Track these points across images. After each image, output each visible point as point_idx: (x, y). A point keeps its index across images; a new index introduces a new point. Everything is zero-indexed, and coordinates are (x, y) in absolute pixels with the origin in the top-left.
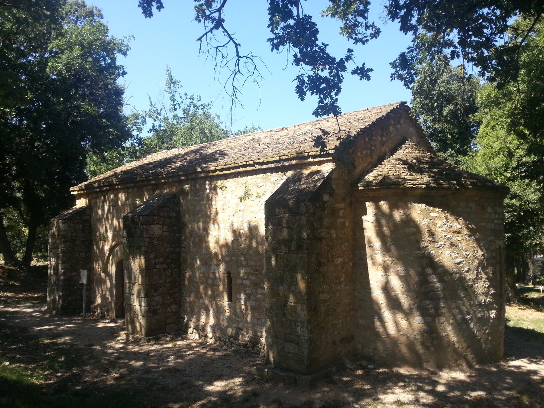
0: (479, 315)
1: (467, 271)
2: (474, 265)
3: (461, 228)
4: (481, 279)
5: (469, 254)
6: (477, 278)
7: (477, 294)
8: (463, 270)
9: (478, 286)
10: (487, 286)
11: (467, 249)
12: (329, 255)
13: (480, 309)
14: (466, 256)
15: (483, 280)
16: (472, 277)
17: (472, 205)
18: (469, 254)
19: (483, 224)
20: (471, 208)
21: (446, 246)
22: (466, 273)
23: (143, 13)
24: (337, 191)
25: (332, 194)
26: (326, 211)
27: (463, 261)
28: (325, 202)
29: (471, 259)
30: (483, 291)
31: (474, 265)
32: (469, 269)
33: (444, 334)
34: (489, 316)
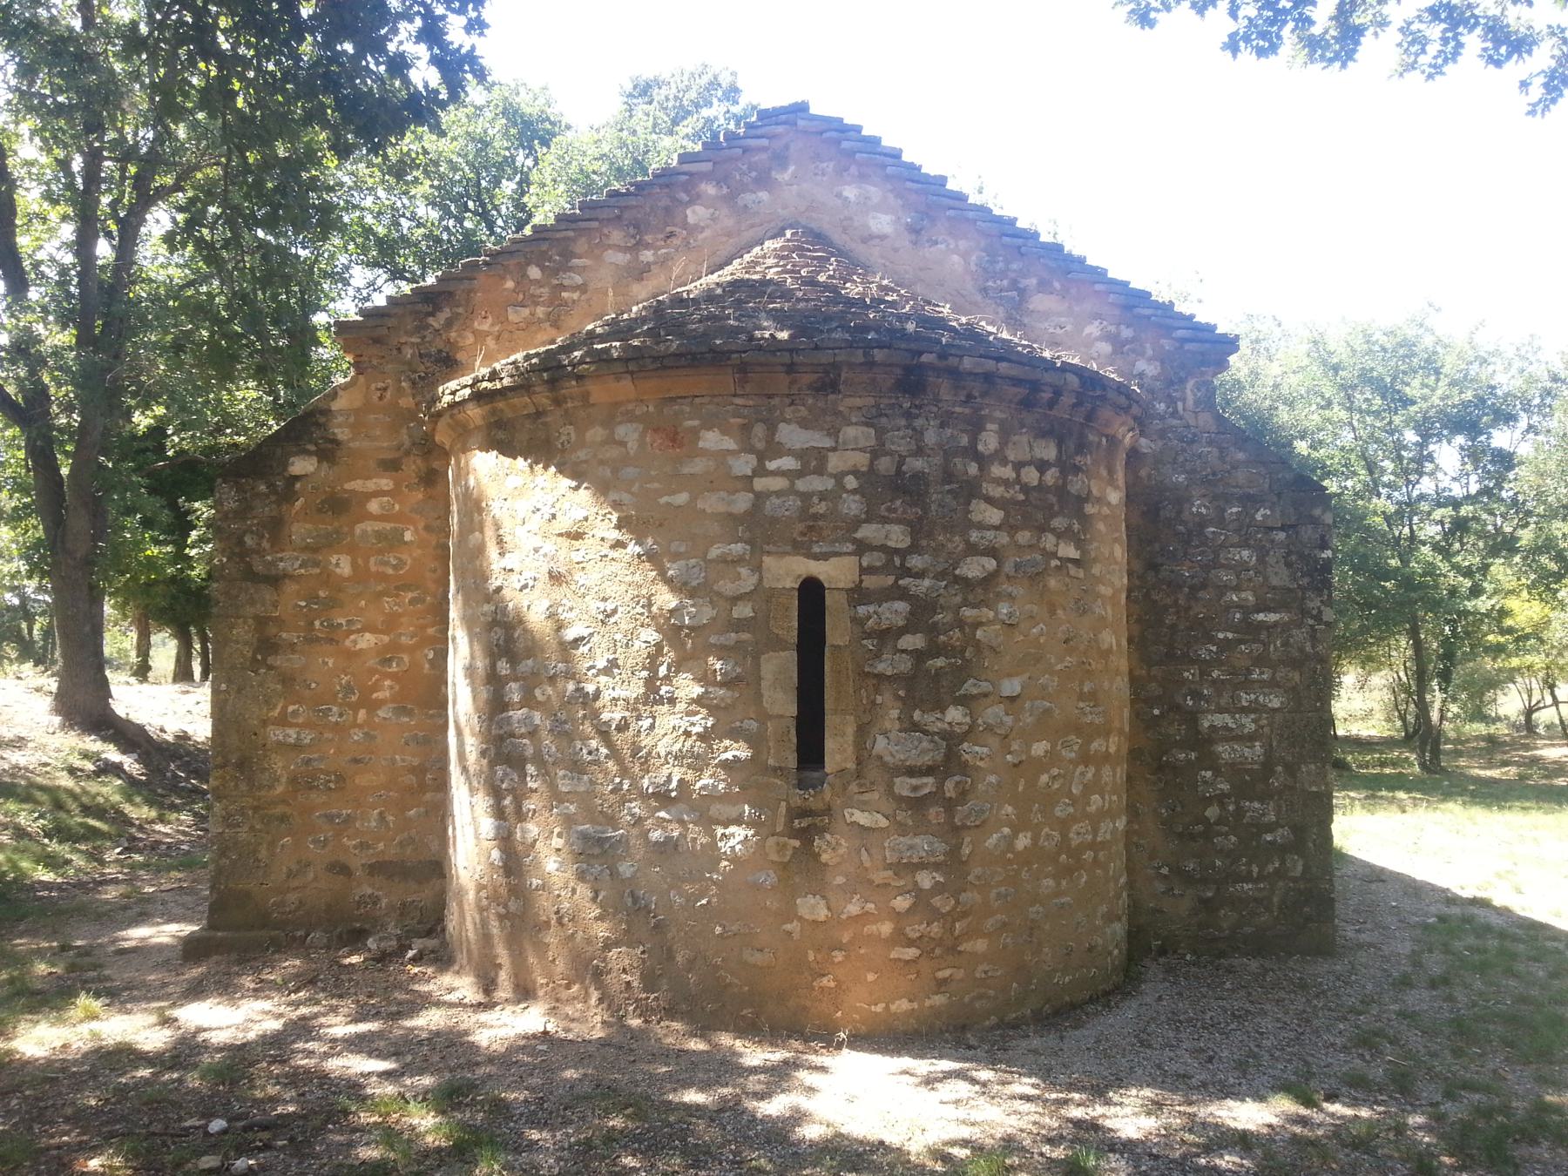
0: (656, 835)
1: (607, 671)
2: (636, 647)
3: (586, 519)
4: (672, 701)
5: (615, 611)
6: (652, 695)
7: (649, 753)
8: (592, 667)
9: (652, 727)
10: (698, 729)
11: (609, 593)
12: (317, 623)
13: (662, 814)
14: (601, 617)
15: (681, 707)
16: (623, 694)
17: (628, 433)
18: (615, 611)
19: (682, 498)
20: (623, 444)
21: (539, 585)
22: (603, 679)
23: (801, 108)
24: (355, 445)
25: (329, 452)
26: (298, 504)
27: (591, 635)
28: (297, 478)
29: (624, 626)
30: (677, 746)
31: (636, 647)
32: (613, 664)
33: (536, 882)
34: (713, 845)
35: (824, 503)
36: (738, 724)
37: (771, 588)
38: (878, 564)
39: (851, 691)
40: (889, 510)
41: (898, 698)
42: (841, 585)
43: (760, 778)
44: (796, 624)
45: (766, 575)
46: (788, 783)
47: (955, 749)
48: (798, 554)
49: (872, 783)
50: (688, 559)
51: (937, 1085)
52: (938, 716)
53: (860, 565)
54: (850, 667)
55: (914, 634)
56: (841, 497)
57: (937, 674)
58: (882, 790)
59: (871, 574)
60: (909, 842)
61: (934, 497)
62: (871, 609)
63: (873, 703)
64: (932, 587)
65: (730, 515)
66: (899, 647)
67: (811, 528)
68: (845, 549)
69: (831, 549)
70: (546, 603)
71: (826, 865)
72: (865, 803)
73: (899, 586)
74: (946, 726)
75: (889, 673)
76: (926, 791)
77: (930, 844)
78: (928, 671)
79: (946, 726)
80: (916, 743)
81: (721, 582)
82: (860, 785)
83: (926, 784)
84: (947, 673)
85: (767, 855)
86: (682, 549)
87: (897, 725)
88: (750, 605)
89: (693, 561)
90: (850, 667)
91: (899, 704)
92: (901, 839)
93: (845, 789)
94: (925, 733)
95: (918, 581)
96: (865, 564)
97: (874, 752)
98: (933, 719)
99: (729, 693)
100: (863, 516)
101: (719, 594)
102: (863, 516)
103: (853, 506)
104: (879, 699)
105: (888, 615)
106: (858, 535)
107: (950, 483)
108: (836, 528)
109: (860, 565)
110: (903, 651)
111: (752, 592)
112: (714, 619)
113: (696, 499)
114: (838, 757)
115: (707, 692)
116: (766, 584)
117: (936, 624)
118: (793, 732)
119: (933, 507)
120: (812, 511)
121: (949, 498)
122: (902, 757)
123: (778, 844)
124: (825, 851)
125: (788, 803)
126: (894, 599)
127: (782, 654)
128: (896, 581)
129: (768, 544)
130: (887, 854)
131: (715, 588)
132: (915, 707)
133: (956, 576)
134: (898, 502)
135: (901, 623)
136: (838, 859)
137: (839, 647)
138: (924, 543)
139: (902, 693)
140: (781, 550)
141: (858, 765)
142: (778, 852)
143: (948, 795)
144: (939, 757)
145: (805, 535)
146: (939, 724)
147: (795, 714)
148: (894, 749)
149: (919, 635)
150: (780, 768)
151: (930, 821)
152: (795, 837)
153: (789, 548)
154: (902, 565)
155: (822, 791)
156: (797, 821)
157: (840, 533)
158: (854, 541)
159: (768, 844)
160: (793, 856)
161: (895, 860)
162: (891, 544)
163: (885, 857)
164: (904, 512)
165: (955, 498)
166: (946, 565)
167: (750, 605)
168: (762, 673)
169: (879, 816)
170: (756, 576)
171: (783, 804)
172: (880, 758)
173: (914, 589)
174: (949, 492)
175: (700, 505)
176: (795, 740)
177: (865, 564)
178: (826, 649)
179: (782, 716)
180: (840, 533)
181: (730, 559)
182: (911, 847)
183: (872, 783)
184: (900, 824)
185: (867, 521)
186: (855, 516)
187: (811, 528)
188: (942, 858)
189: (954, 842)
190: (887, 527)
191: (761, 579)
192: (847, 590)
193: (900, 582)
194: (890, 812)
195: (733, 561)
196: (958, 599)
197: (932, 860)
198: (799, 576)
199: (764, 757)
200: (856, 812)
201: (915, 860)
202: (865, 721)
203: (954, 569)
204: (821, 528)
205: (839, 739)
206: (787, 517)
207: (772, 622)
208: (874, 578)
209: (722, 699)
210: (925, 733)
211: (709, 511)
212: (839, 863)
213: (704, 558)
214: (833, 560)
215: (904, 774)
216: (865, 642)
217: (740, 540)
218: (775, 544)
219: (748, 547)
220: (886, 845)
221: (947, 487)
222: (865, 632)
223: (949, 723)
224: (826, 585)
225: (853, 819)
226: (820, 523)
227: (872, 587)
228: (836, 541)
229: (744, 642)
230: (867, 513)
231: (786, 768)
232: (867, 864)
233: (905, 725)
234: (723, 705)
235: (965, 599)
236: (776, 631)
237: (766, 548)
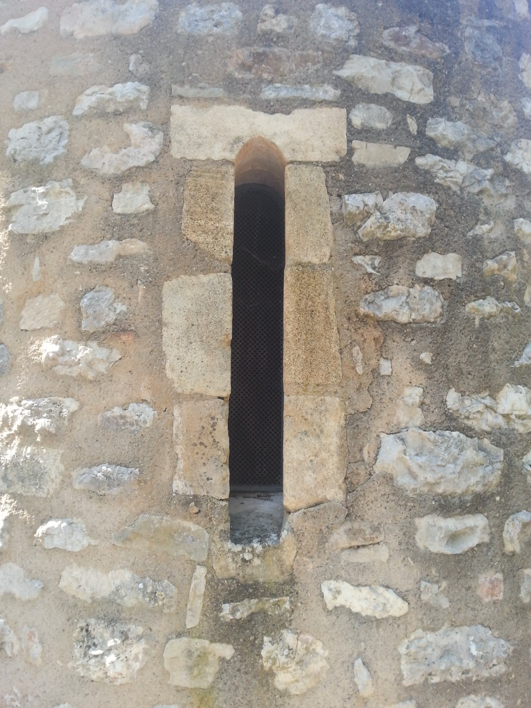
35: (282, 18)
36: (117, 411)
37: (184, 160)
38: (380, 125)
39: (335, 349)
40: (397, 38)
41: (419, 364)
42: (315, 156)
43: (156, 519)
44: (229, 224)
45: (176, 136)
46: (210, 529)
47: (518, 463)
48: (236, 101)
49: (376, 529)
50: (41, 119)
51: (362, 588)
52: (488, 401)
53: (349, 122)
54: (332, 303)
55: (444, 252)
56: (313, 9)
57: (484, 327)
58: (394, 544)
59: (367, 139)
60: (444, 642)
61: (468, 32)
62: (371, 199)
63: (375, 372)
64: (471, 176)
65: (116, 37)
66: (419, 273)
67: (259, 58)
68: (320, 95)
69: (296, 94)
70: (309, 420)
71: (285, 694)
72: (363, 568)
73: (416, 169)
74: (501, 421)
75: (403, 318)
76: (472, 542)
77: (481, 642)
78: (469, 320)
79: (501, 421)
80: (455, 451)
81: (95, 152)
82: (352, 533)
83: (472, 529)
84: (497, 326)
85: (166, 674)
86: (33, 104)
87: (419, 418)
88: (146, 189)
89: (49, 122)
90: (332, 303)
91: (421, 378)
92: (430, 637)
93: (323, 539)
94: (468, 431)
95: (448, 163)
96: (357, 122)
97: (378, 469)
98: (481, 408)
99: (102, 353)
100: (353, 43)
101: (91, 174)
102: (353, 43)
103: (335, 24)
104: (385, 368)
105: (399, 214)
106: (345, 72)
107: (490, 17)
108: (305, 60)
109: (349, 122)
110: (427, 281)
111: (149, 166)
112: (79, 217)
113: (59, 16)
114: (309, 478)
115: (63, 353)
116: (176, 152)
117: (477, 239)
118: (223, 427)
119: (468, 47)
120: (262, 27)
121: (490, 40)
122: (430, 477)
123: (190, 653)
124: (283, 668)
125: (210, 570)
126: (407, 189)
127: (204, 278)
128: (411, 159)
129: (182, 83)
130: (405, 667)
131: (84, 162)
132: (449, 383)
133: (506, 165)
134: (412, 30)
135: (423, 231)
136: (309, 683)
137: (312, 266)
138: (455, 101)
139: (426, 357)
140: (205, 93)
141: (348, 492)
142: (190, 669)
143: (509, 548)
144: (494, 478)
145: (249, 69)
146: (490, 417)
147: (227, 392)
148: (414, 462)
149: (452, 257)
150: (196, 499)
151: (479, 600)
152: (224, 639)
153: (219, 92)
154: (421, 133)
155: (278, 546)
156: (227, 608)
157: (311, 68)
158: (338, 83)
159: (167, 655)
160: (221, 673)
161: (419, 679)
162: (403, 95)
163: (401, 675)
164: (421, 46)
165: (500, 41)
166: (492, 144)
167: (146, 189)
168: (165, 314)
169: (390, 595)
170: (159, 137)
171: (201, 572)
172: (389, 479)
173: (441, 174)
174: (489, 29)
175: (65, 26)
176: (225, 442)
177: (357, 122)
178: (287, 272)
179: (202, 397)
180: (311, 68)
181: (111, 108)
182: (446, 652)
183: (376, 529)
184: (427, 607)
185: (360, 50)
186: (338, 40)
187: (259, 58)
188: (501, 669)
189: (519, 634)
190: (395, 66)
191: (166, 144)
192: (327, 167)
193: (419, 161)
194: (407, 585)
195: (117, 114)
196: (510, 204)
197: (485, 674)
198: (238, 140)
199: (165, 476)
200: (346, 588)
201: (456, 677)
202: (362, 406)
203: (504, 153)
204: (279, 59)
205: (311, 441)
206: (218, 37)
207: (186, 220)
208: (373, 148)
209: (90, 365)
210: (468, 431)
211: (80, 35)
212: (312, 690)
213: (68, 115)
214: (299, 114)
215: (433, 510)
216: (358, 259)
217: (131, 77)
218: (193, 83)
219: (145, 88)
220: (402, 650)
221: (487, 23)
222: (358, 241)
223: (506, 416)
224: (287, 156)
225: (340, 601)
226: (276, 50)
227: (370, 164)
228: (306, 80)
229: (133, 257)
230: (359, 37)
231: (208, 499)
232: (367, 691)
233: (433, 418)
234: (91, 376)
235: (520, 206)
236: (193, 237)
237: (178, 90)
